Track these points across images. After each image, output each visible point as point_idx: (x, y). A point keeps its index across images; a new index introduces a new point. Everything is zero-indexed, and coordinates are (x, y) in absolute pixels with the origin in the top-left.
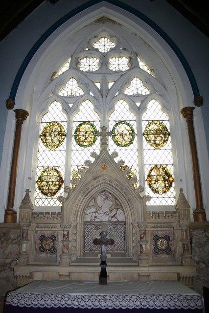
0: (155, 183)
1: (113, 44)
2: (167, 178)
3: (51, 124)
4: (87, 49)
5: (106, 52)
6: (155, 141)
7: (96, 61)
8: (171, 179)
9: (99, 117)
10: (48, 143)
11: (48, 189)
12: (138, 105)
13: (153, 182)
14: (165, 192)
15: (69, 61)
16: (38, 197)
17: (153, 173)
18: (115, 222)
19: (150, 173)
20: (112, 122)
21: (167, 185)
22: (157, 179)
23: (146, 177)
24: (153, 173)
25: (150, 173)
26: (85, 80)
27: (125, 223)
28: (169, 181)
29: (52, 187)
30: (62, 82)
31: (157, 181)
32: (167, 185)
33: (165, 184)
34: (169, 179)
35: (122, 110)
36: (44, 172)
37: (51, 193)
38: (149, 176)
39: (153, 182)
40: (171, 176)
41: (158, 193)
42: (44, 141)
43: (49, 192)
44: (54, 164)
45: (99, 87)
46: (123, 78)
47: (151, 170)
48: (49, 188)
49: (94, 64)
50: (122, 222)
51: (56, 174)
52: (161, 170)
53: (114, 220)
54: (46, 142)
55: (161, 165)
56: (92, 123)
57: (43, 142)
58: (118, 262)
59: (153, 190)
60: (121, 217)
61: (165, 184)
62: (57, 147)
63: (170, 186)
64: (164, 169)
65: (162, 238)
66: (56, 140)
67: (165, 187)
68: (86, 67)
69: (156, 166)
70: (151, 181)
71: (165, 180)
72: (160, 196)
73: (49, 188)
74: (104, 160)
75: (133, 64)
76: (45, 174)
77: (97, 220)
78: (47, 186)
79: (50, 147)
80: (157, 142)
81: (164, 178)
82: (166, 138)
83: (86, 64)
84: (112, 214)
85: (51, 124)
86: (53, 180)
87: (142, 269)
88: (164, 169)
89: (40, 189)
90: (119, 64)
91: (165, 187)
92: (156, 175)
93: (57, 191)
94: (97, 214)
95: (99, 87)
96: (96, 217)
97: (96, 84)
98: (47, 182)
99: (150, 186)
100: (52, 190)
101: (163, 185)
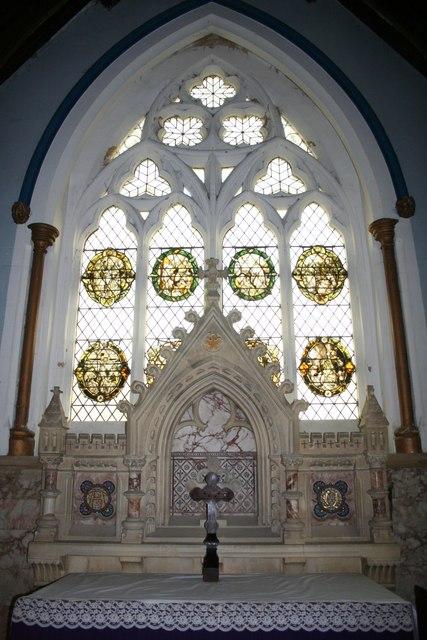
0: (316, 375)
1: (231, 90)
2: (341, 364)
3: (105, 254)
4: (178, 100)
5: (216, 106)
6: (316, 288)
7: (195, 125)
8: (349, 366)
9: (201, 240)
10: (98, 293)
11: (99, 387)
12: (283, 214)
13: (313, 372)
14: (338, 392)
15: (142, 125)
17: (313, 354)
18: (236, 454)
19: (307, 353)
20: (228, 250)
21: (341, 378)
23: (298, 363)
24: (313, 354)
25: (307, 353)
26: (174, 163)
27: (255, 456)
29: (106, 382)
30: (127, 167)
31: (321, 369)
33: (338, 376)
34: (344, 365)
35: (249, 226)
36: (90, 351)
37: (104, 394)
38: (305, 360)
39: (313, 372)
40: (350, 360)
41: (323, 394)
42: (91, 288)
43: (100, 393)
44: (111, 334)
45: (202, 178)
46: (252, 160)
47: (308, 349)
48: (100, 383)
50: (249, 454)
51: (114, 356)
52: (328, 347)
53: (234, 449)
54: (94, 291)
56: (188, 251)
57: (88, 291)
58: (241, 536)
59: (312, 388)
60: (246, 444)
61: (338, 376)
62: (117, 301)
63: (348, 380)
64: (334, 345)
65: (330, 486)
66: (114, 285)
67: (338, 382)
68: (175, 136)
69: (319, 339)
70: (308, 370)
71: (337, 368)
72: (327, 400)
73: (100, 383)
74: (213, 327)
75: (272, 132)
76: (93, 356)
77: (198, 450)
78: (95, 380)
79: (103, 301)
80: (321, 291)
81: (335, 365)
84: (230, 438)
85: (105, 254)
87: (291, 549)
88: (334, 345)
89: (81, 386)
90: (244, 130)
91: (338, 382)
92: (319, 357)
93: (117, 391)
94: (198, 438)
95: (202, 178)
96: (196, 444)
97: (196, 171)
98: (97, 373)
99: (307, 381)
100: (106, 388)
101: (333, 378)
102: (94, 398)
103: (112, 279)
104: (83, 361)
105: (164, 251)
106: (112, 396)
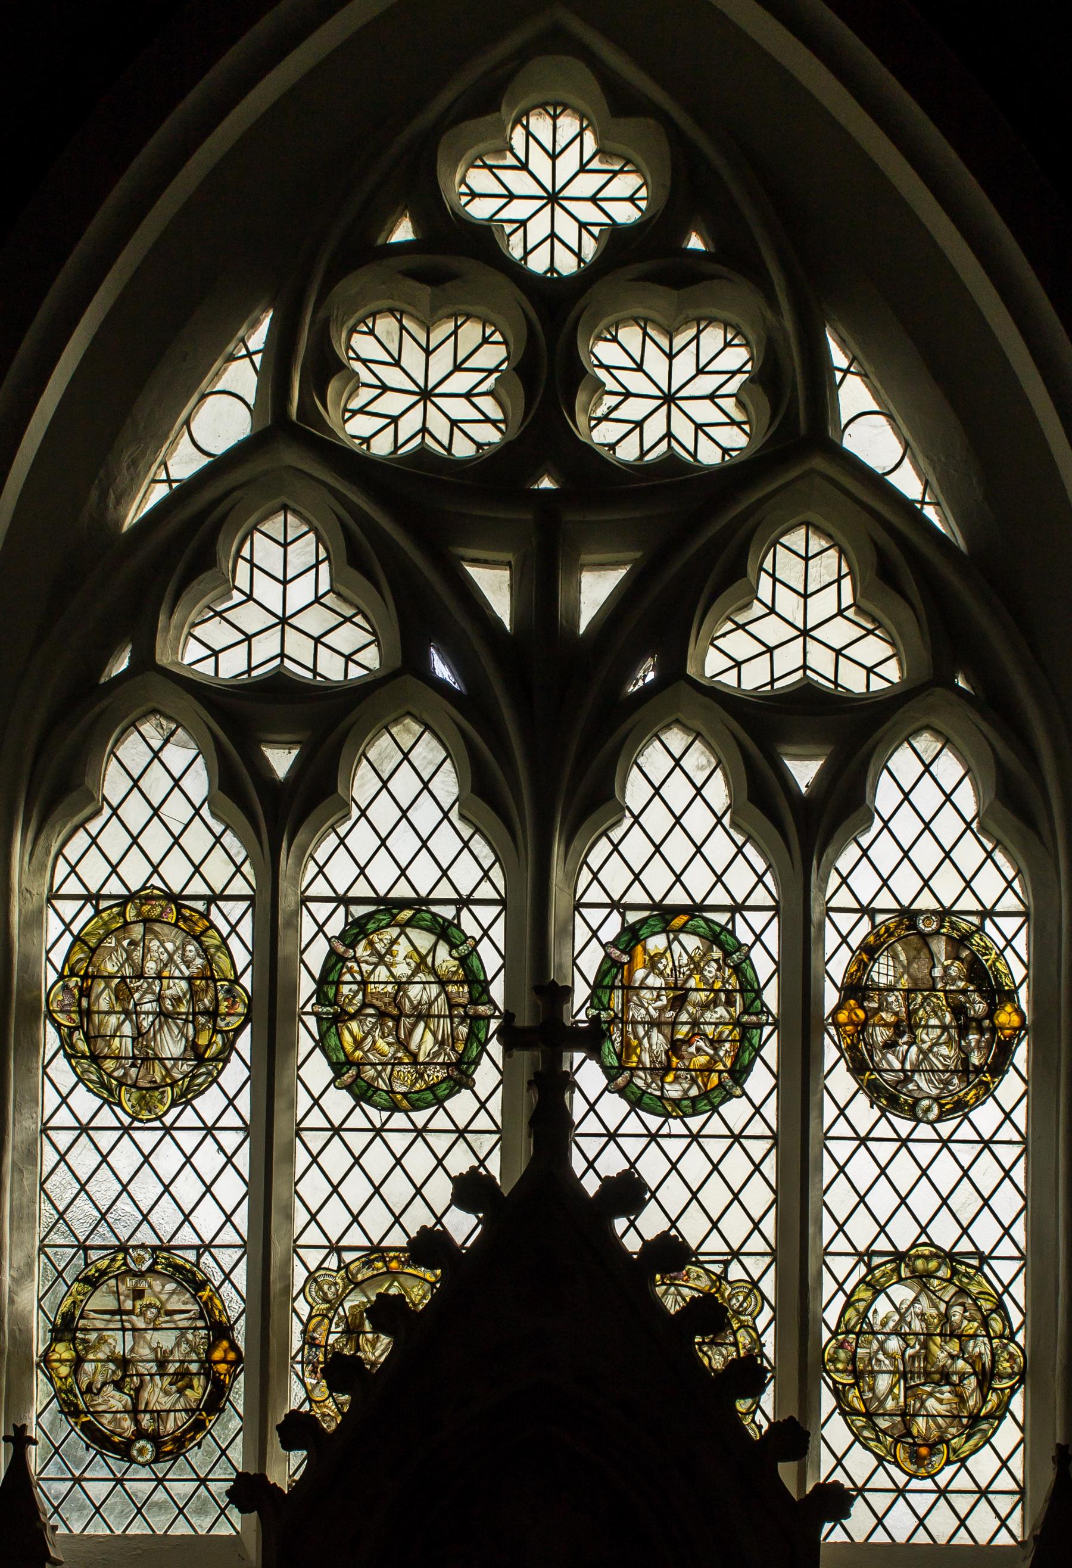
0: (890, 1045)
1: (627, 183)
2: (980, 1007)
3: (131, 913)
4: (403, 232)
5: (567, 265)
6: (906, 1415)
8: (1006, 1017)
9: (496, 874)
10: (109, 1065)
11: (134, 1412)
13: (881, 1035)
15: (258, 339)
16: (63, 1117)
17: (883, 972)
20: (595, 916)
21: (975, 1059)
22: (911, 1014)
23: (831, 998)
24: (883, 972)
28: (994, 1029)
29: (156, 1395)
32: (975, 1059)
33: (965, 1055)
34: (991, 1014)
36: (93, 1282)
37: (155, 1438)
40: (1010, 996)
41: (912, 1113)
42: (82, 1046)
43: (140, 1434)
45: (501, 605)
48: (135, 1401)
49: (462, 382)
52: (940, 947)
54: (95, 1059)
55: (945, 913)
56: (448, 912)
59: (874, 1091)
61: (965, 1055)
62: (185, 1098)
63: (999, 1066)
64: (959, 942)
67: (965, 1070)
68: (392, 404)
69: (907, 915)
70: (862, 1027)
71: (964, 1022)
72: (924, 1131)
73: (135, 1401)
76: (102, 1300)
78: (119, 1386)
81: (958, 1010)
82: (993, 1398)
83: (392, 377)
85: (131, 913)
86: (166, 1340)
89: (70, 1410)
91: (965, 1070)
92: (904, 982)
93: (199, 1426)
95: (501, 605)
97: (475, 573)
98: (124, 1363)
100: (159, 1415)
102: (124, 1450)
103: (163, 1015)
104: (68, 1318)
105: (359, 911)
106: (180, 1443)
